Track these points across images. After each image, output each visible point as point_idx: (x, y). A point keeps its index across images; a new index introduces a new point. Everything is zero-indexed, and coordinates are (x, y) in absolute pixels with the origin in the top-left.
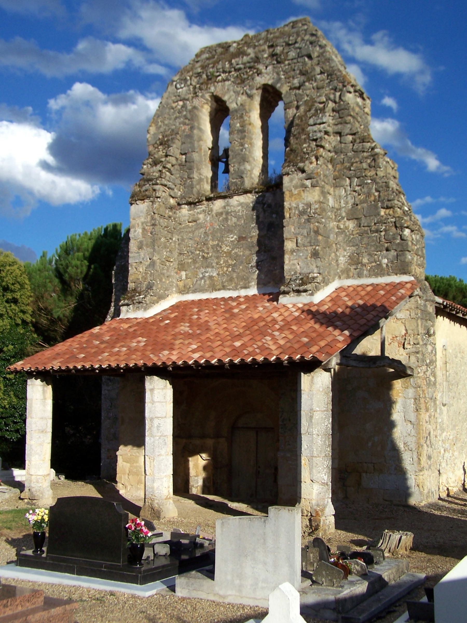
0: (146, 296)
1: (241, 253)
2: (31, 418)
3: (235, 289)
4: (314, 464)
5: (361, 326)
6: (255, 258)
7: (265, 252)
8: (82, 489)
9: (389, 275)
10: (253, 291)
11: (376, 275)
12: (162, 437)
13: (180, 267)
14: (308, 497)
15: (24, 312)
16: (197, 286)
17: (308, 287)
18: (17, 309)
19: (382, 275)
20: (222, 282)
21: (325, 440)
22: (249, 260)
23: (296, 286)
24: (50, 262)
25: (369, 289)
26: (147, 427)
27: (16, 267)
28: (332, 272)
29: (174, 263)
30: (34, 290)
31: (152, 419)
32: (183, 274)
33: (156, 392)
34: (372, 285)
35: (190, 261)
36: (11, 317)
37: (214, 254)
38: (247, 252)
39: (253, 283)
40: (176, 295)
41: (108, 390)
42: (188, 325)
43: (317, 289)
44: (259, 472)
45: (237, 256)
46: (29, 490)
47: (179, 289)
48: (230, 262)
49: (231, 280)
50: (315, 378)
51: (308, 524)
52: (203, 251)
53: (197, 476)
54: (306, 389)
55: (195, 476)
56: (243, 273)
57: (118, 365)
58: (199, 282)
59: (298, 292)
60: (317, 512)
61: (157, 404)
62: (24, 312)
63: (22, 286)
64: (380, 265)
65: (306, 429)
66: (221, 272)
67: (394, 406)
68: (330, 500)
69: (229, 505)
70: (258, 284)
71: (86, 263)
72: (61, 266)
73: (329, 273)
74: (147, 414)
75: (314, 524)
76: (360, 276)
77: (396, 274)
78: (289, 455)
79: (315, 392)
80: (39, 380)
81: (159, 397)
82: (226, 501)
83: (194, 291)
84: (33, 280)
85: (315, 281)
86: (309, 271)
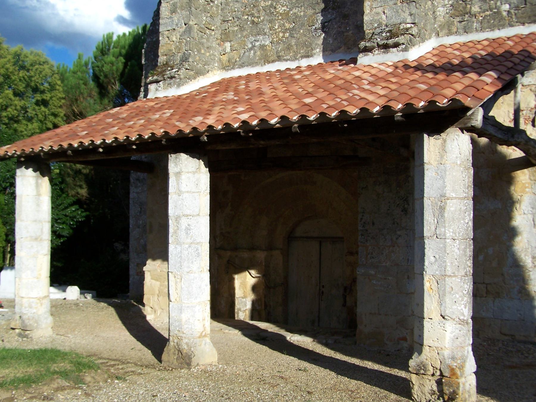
0: (179, 69)
1: (302, 14)
2: (22, 221)
3: (295, 59)
4: (448, 289)
5: (509, 69)
6: (320, 18)
7: (333, 9)
8: (100, 313)
9: (512, 26)
10: (318, 59)
11: (492, 28)
12: (193, 245)
13: (223, 37)
14: (436, 344)
15: (55, 115)
16: (245, 59)
17: (401, 39)
18: (47, 111)
19: (501, 26)
20: (277, 52)
21: (465, 248)
22: (313, 22)
23: (382, 40)
24: (86, 65)
25: (486, 43)
26: (171, 230)
27: (46, 66)
28: (428, 27)
29: (216, 32)
30: (66, 92)
31: (178, 218)
32: (228, 45)
33: (184, 177)
34: (486, 40)
35: (236, 29)
36: (41, 121)
37: (266, 17)
38: (310, 12)
39: (318, 50)
40: (219, 72)
41: (137, 193)
42: (233, 93)
43: (411, 44)
44: (323, 293)
45: (296, 17)
46: (20, 317)
47: (222, 65)
48: (287, 25)
49: (289, 48)
50: (448, 142)
51: (435, 388)
52: (252, 15)
53: (245, 297)
54: (432, 162)
55: (243, 298)
56: (304, 38)
57: (128, 137)
58: (247, 54)
59: (386, 47)
60: (452, 370)
61: (185, 195)
62: (55, 115)
63: (52, 88)
64: (499, 13)
65: (433, 228)
66: (275, 40)
67: (518, 206)
68: (470, 348)
69: (288, 338)
70: (324, 51)
71: (122, 59)
72: (97, 69)
73: (425, 25)
74: (172, 211)
75: (447, 390)
76: (466, 31)
77: (523, 24)
78: (373, 272)
79: (448, 166)
80: (30, 170)
81: (189, 184)
82: (283, 332)
83: (241, 66)
84: (66, 82)
85: (410, 32)
86: (399, 22)
